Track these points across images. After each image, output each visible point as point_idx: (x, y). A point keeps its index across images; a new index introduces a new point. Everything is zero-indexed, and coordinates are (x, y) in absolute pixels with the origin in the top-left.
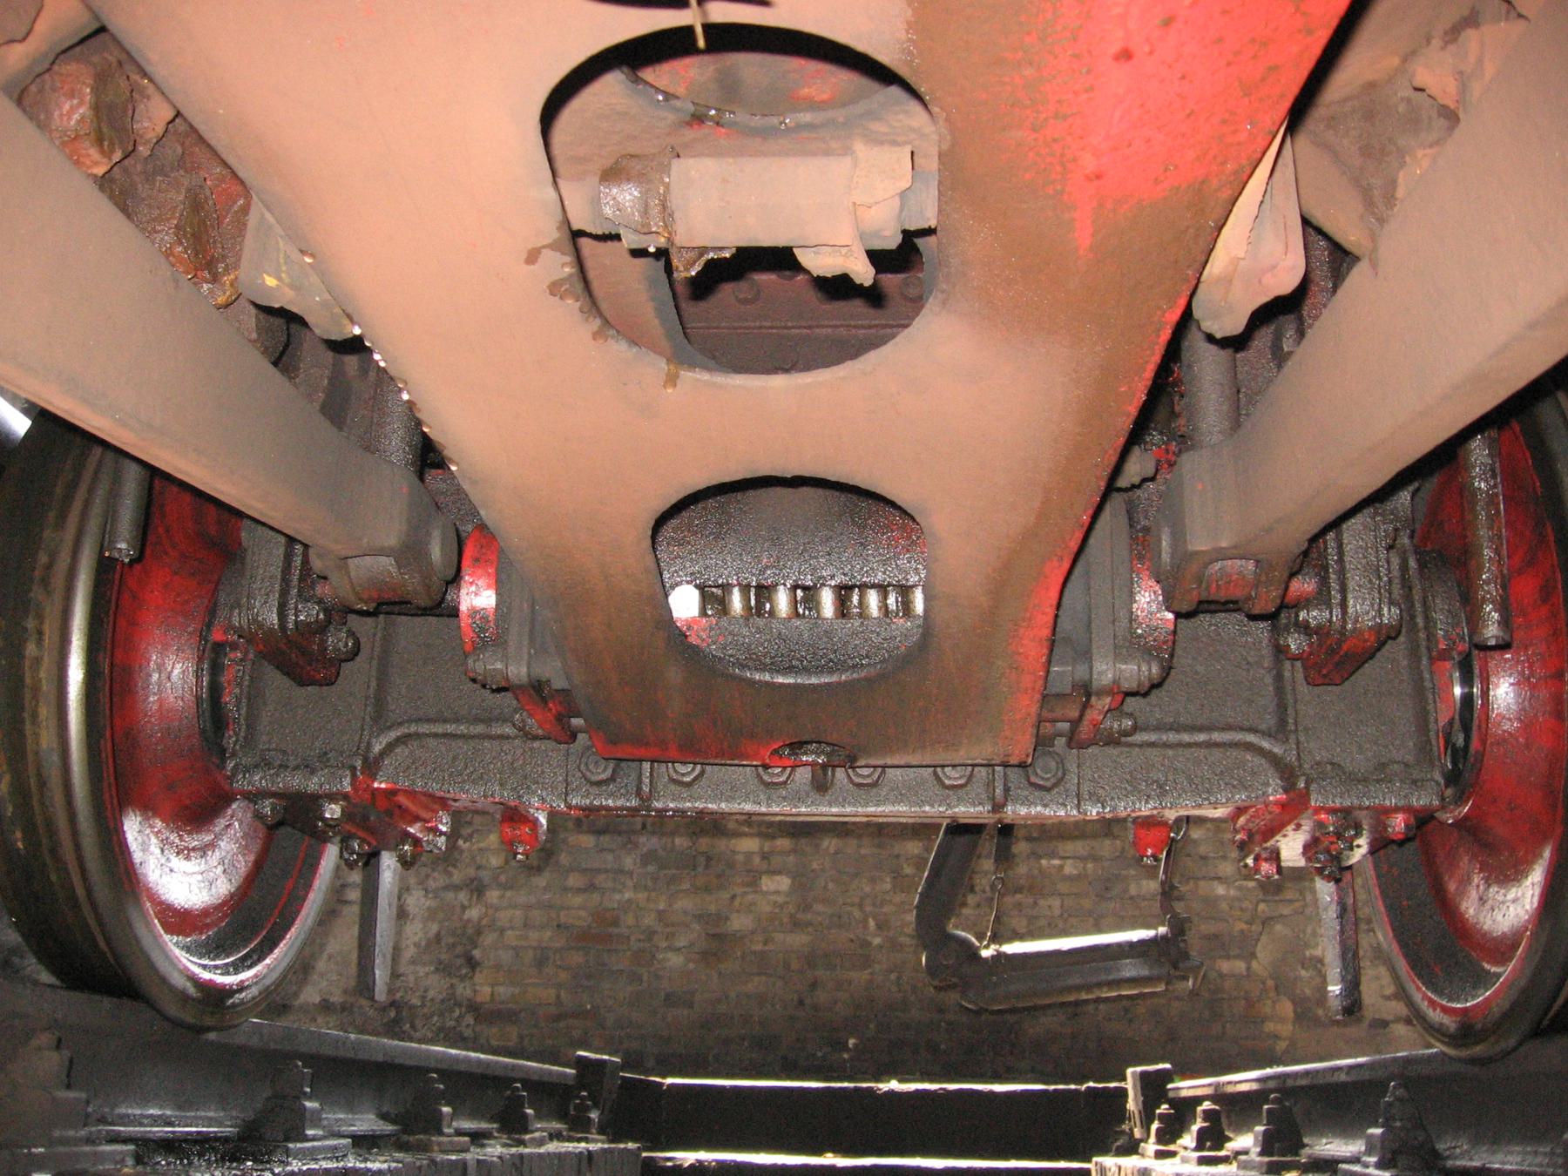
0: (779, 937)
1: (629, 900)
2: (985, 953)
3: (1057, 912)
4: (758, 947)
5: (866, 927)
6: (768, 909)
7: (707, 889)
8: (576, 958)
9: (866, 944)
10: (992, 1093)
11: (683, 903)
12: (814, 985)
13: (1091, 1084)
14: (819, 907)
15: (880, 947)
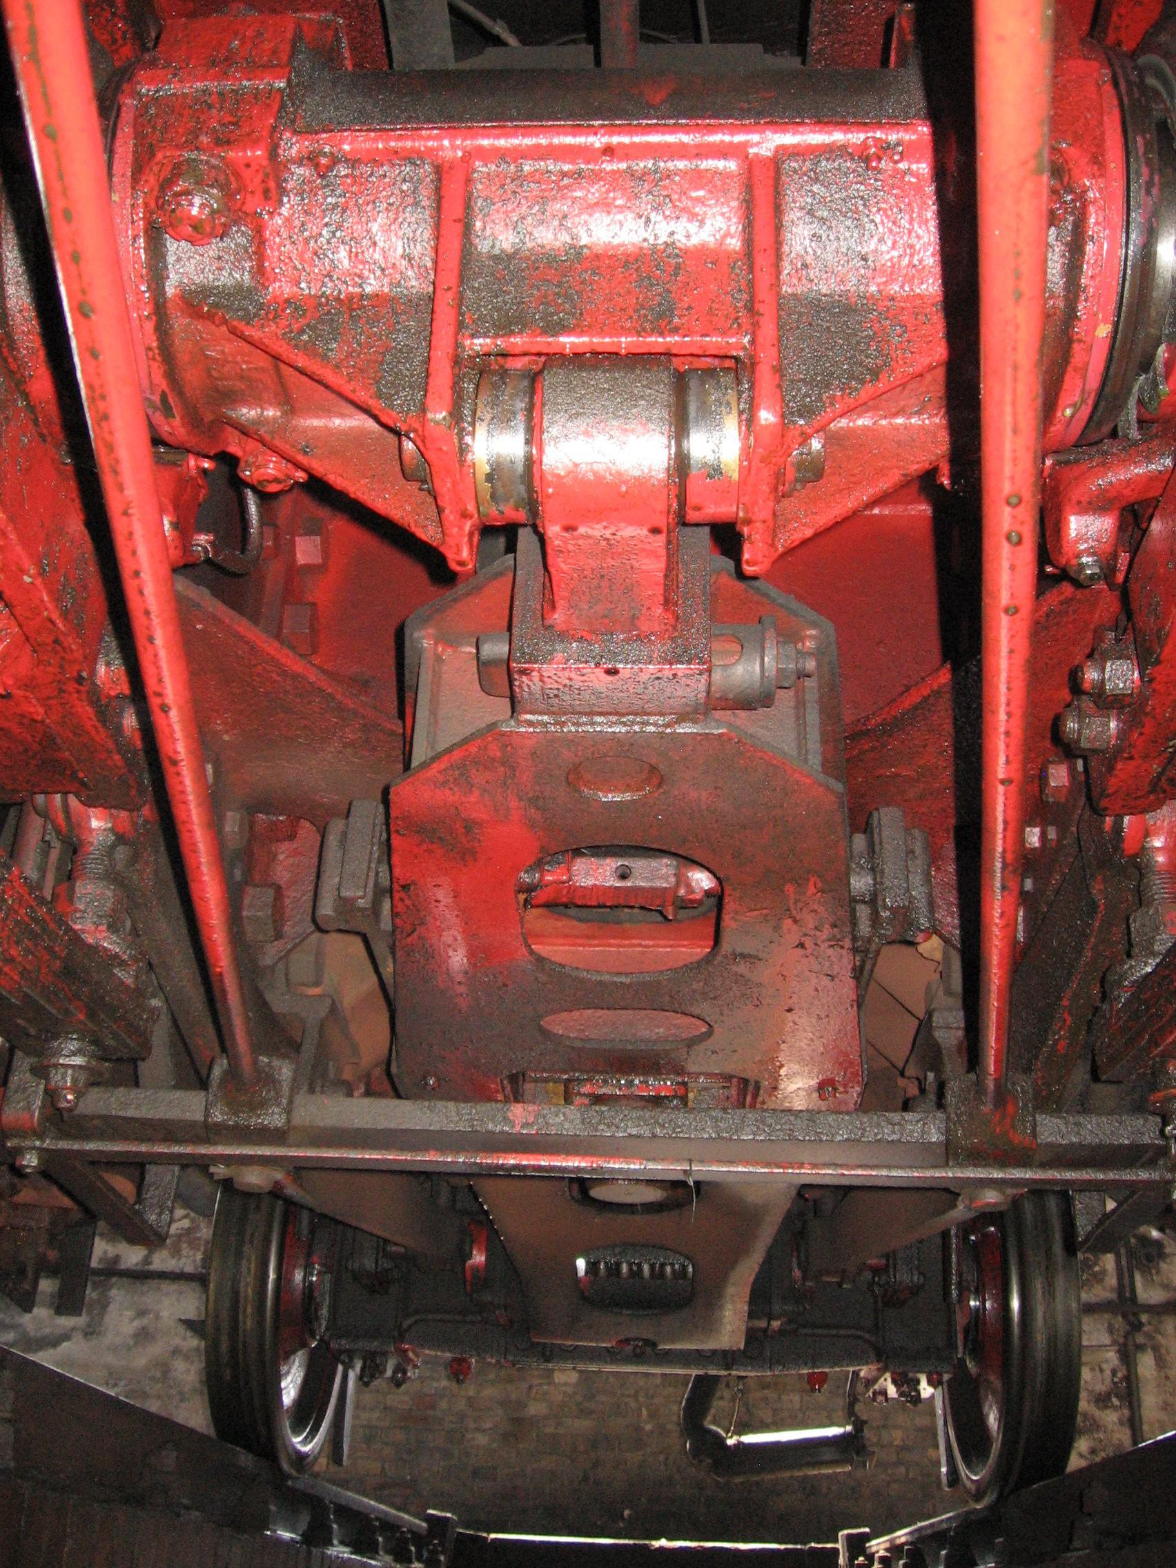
0: (569, 1421)
1: (444, 1388)
2: (730, 1442)
3: (798, 1406)
4: (550, 1430)
5: (640, 1415)
6: (560, 1398)
7: (510, 1380)
8: (399, 1436)
9: (638, 1429)
10: (738, 1550)
11: (488, 1392)
12: (596, 1464)
13: (813, 1545)
14: (603, 1398)
15: (652, 1432)
